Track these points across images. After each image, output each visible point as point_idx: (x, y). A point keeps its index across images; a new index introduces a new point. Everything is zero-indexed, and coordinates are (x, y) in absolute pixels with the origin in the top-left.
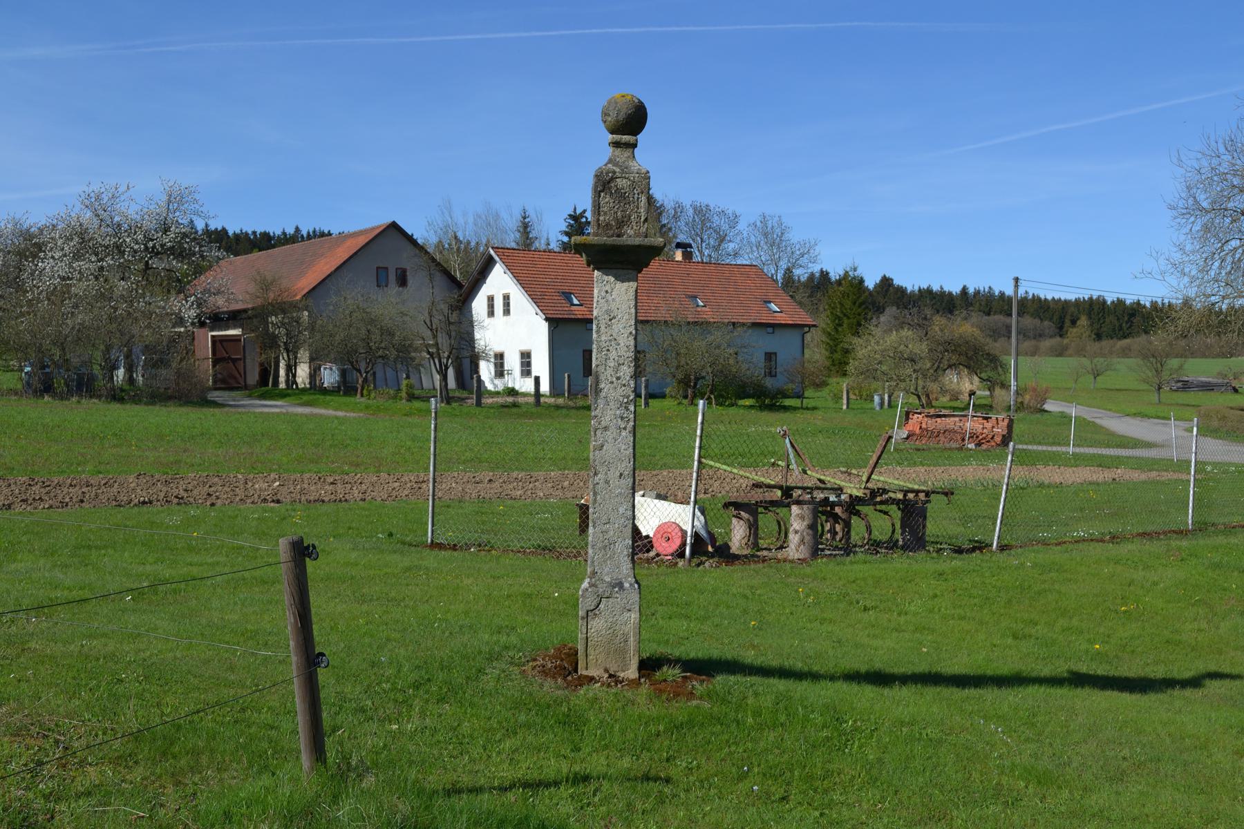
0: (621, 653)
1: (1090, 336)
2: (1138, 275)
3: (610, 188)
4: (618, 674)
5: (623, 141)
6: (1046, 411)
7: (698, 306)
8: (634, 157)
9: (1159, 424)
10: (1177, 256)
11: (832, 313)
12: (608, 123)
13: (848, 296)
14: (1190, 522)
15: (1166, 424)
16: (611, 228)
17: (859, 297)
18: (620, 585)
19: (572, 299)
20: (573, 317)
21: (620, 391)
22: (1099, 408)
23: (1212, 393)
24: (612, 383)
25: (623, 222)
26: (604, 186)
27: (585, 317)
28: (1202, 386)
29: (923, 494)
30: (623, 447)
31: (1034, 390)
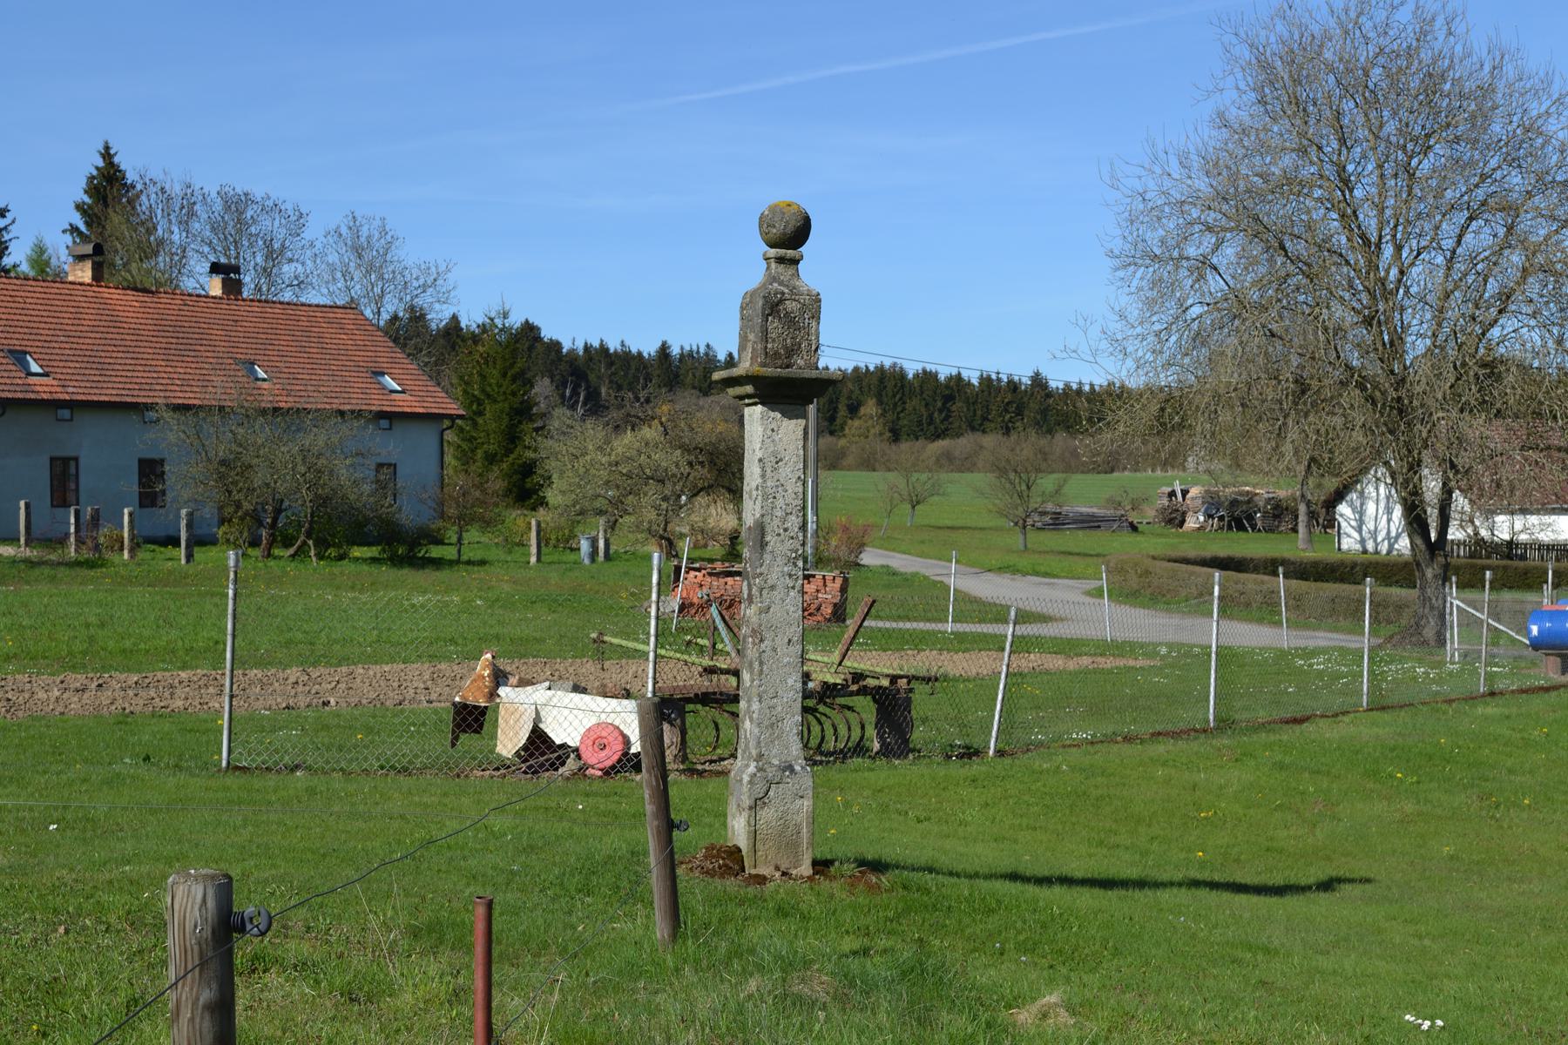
0: (793, 846)
1: (881, 434)
2: (1058, 354)
3: (778, 311)
4: (790, 871)
5: (788, 256)
6: (864, 566)
7: (257, 379)
9: (1040, 584)
10: (1115, 326)
11: (465, 392)
12: (770, 235)
14: (1211, 718)
15: (1053, 584)
17: (512, 365)
18: (791, 768)
19: (28, 362)
20: (33, 396)
21: (789, 544)
22: (940, 559)
23: (1098, 533)
24: (779, 535)
27: (56, 396)
28: (1082, 522)
29: (905, 680)
30: (792, 609)
31: (846, 529)
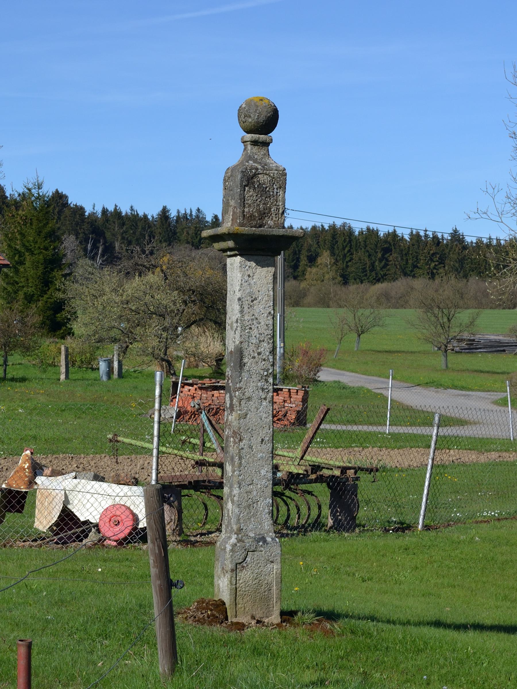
1: (333, 279)
2: (472, 215)
4: (263, 620)
8: (269, 155)
11: (9, 246)
13: (31, 224)
15: (469, 395)
16: (254, 219)
21: (262, 365)
22: (380, 376)
23: (503, 355)
24: (254, 357)
25: (264, 213)
26: (248, 181)
28: (491, 347)
29: (352, 471)
30: (264, 415)
31: (305, 353)
